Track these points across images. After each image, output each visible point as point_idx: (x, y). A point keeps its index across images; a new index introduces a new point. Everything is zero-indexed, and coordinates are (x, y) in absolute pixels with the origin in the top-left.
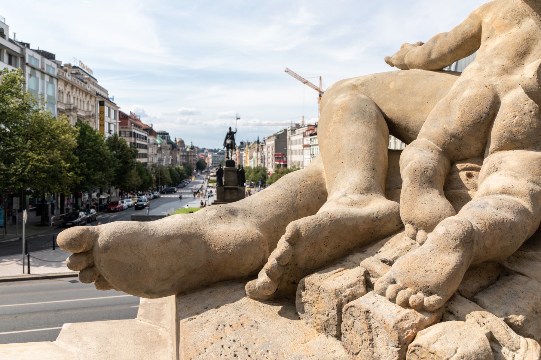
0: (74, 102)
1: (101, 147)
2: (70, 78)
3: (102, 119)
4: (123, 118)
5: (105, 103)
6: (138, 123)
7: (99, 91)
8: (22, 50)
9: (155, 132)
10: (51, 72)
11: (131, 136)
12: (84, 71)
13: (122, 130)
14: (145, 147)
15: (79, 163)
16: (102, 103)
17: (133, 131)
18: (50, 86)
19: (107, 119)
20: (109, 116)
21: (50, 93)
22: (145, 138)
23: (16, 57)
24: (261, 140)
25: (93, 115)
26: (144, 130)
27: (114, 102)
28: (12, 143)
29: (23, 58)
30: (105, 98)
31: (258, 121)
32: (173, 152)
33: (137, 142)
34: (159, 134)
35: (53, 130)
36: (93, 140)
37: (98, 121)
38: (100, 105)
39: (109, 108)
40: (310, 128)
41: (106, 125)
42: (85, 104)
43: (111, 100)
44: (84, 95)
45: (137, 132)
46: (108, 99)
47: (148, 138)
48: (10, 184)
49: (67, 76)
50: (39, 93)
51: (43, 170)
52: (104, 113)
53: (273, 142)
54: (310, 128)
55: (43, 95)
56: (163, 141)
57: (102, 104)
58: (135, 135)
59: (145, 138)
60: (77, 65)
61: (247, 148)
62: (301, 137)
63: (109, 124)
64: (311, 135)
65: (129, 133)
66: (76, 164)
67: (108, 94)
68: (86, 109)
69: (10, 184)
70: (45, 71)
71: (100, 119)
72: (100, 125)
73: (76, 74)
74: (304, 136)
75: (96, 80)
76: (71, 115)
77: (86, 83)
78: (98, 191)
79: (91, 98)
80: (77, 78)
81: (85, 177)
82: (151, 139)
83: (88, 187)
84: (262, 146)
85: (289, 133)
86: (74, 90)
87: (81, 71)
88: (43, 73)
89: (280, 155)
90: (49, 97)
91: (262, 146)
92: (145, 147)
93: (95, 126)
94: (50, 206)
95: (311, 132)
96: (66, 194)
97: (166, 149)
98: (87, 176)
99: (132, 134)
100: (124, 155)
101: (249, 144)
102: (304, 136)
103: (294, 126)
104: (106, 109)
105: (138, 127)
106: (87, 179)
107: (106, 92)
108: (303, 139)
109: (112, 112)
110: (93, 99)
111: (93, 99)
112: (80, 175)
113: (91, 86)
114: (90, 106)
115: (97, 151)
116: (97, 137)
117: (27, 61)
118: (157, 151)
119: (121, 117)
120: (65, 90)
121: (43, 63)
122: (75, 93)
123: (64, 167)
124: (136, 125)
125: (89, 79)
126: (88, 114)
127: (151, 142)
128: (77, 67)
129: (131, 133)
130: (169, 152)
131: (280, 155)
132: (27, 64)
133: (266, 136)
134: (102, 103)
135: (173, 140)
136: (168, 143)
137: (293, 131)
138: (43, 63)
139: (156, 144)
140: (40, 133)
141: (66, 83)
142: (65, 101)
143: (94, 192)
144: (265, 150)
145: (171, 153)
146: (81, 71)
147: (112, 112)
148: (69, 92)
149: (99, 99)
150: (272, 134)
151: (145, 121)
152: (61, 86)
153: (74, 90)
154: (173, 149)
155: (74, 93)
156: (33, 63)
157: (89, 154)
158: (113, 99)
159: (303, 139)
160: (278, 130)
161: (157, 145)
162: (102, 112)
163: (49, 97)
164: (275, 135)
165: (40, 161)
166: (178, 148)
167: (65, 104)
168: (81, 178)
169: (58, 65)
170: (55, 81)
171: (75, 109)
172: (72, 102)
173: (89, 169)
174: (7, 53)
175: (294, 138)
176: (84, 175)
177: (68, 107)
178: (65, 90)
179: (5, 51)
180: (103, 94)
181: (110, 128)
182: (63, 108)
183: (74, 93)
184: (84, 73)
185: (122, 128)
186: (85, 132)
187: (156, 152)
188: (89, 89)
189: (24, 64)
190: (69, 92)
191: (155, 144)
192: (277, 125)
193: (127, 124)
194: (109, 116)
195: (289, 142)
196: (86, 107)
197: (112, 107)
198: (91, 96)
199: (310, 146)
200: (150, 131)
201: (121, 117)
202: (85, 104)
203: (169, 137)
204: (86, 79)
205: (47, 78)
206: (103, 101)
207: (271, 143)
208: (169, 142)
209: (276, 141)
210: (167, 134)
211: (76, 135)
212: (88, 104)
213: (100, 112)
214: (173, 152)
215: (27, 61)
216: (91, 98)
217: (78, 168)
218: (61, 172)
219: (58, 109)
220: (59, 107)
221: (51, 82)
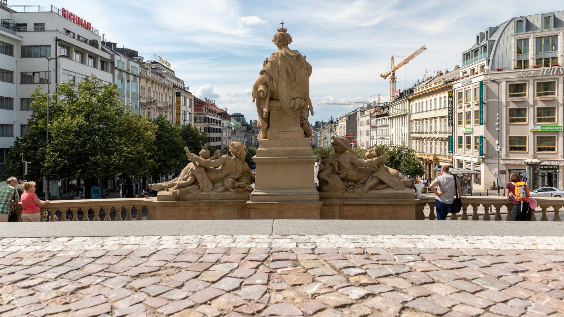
0: (154, 95)
1: (175, 138)
2: (150, 75)
3: (178, 109)
4: (198, 104)
5: (181, 93)
6: (212, 108)
7: (176, 82)
8: (112, 56)
9: (229, 115)
10: (135, 73)
11: (205, 121)
12: (163, 66)
13: (197, 116)
14: (219, 131)
15: (157, 151)
16: (178, 94)
17: (208, 116)
18: (134, 84)
19: (183, 108)
20: (185, 105)
21: (134, 90)
22: (219, 122)
23: (107, 63)
24: (334, 120)
25: (170, 106)
26: (218, 114)
27: (189, 91)
28: (111, 140)
29: (113, 63)
30: (181, 89)
31: (331, 99)
32: (248, 134)
33: (211, 126)
34: (233, 116)
35: (139, 129)
36: (169, 132)
37: (175, 111)
38: (177, 96)
39: (185, 98)
40: (377, 109)
41: (182, 112)
42: (164, 96)
43: (187, 90)
44: (162, 88)
45: (211, 117)
46: (184, 89)
47: (222, 122)
48: (110, 172)
49: (148, 74)
50: (125, 91)
51: (132, 160)
52: (180, 103)
53: (345, 123)
54: (377, 109)
55: (128, 93)
56: (237, 123)
57: (178, 95)
58: (210, 120)
59: (219, 122)
60: (157, 61)
61: (321, 128)
62: (369, 118)
63: (185, 114)
64: (377, 116)
65: (203, 118)
66: (155, 152)
67: (184, 84)
68: (164, 101)
69: (110, 172)
70: (130, 72)
71: (177, 109)
72: (177, 114)
73: (156, 68)
74: (372, 117)
75: (173, 72)
76: (152, 108)
77: (164, 78)
78: (174, 174)
79: (168, 91)
80: (158, 71)
81: (162, 163)
82: (225, 122)
83: (165, 172)
84: (335, 126)
85: (358, 114)
86: (154, 85)
87: (160, 66)
88: (128, 73)
89: (351, 135)
90: (133, 93)
91: (335, 126)
92: (219, 131)
93: (171, 118)
94: (135, 187)
95: (377, 113)
96: (148, 177)
97: (240, 131)
98: (165, 164)
99: (206, 120)
100: (196, 142)
101: (323, 123)
102: (372, 117)
103: (366, 106)
104: (182, 99)
105: (214, 112)
106: (163, 164)
107: (182, 82)
108: (371, 120)
109: (188, 100)
110: (170, 91)
111: (170, 91)
112: (158, 162)
113: (169, 78)
114: (168, 98)
115: (171, 141)
116: (173, 129)
117: (116, 66)
118: (232, 134)
119: (196, 104)
120: (147, 86)
121: (128, 65)
122: (155, 88)
123: (146, 156)
124: (210, 111)
125: (167, 74)
126: (166, 105)
127: (225, 125)
128: (157, 63)
129: (205, 118)
130: (244, 134)
131: (351, 135)
132: (116, 68)
133: (339, 117)
134: (178, 94)
135: (248, 121)
136: (243, 125)
137: (362, 111)
138: (128, 65)
139: (230, 127)
140: (130, 131)
141: (147, 80)
142: (146, 96)
143: (171, 174)
144: (338, 130)
145: (246, 136)
146: (160, 66)
147: (188, 100)
148: (150, 88)
149: (176, 90)
150: (344, 115)
151: (220, 106)
152: (143, 83)
153: (154, 85)
154: (248, 131)
155: (154, 88)
156: (120, 67)
157: (166, 143)
158: (188, 88)
159: (371, 120)
160: (350, 109)
161: (231, 128)
162: (178, 103)
163: (133, 93)
164: (346, 116)
165: (130, 153)
166: (253, 129)
167: (147, 98)
168: (159, 164)
169: (142, 64)
170: (138, 79)
171: (154, 102)
172: (152, 96)
173: (166, 156)
174: (100, 60)
175: (362, 119)
176: (162, 161)
177: (149, 100)
178: (147, 86)
179: (99, 59)
180: (180, 85)
181: (187, 116)
182: (144, 102)
183: (154, 88)
184: (163, 68)
185: (198, 114)
186: (161, 124)
187: (230, 135)
188: (166, 83)
189: (114, 68)
190: (150, 88)
191: (229, 127)
192: (350, 103)
193: (202, 111)
194: (185, 105)
195: (358, 123)
196: (164, 98)
197: (187, 96)
198: (168, 89)
199: (376, 127)
200: (224, 115)
201: (196, 104)
202: (164, 96)
203: (245, 119)
204: (164, 74)
205: (131, 78)
206: (179, 91)
207: (343, 123)
208: (244, 124)
209: (347, 122)
210: (243, 116)
211: (155, 131)
212: (166, 96)
213: (177, 102)
214: (248, 134)
215: (116, 66)
216: (168, 91)
217: (157, 155)
218: (144, 159)
219: (140, 103)
220: (141, 101)
221: (135, 81)
